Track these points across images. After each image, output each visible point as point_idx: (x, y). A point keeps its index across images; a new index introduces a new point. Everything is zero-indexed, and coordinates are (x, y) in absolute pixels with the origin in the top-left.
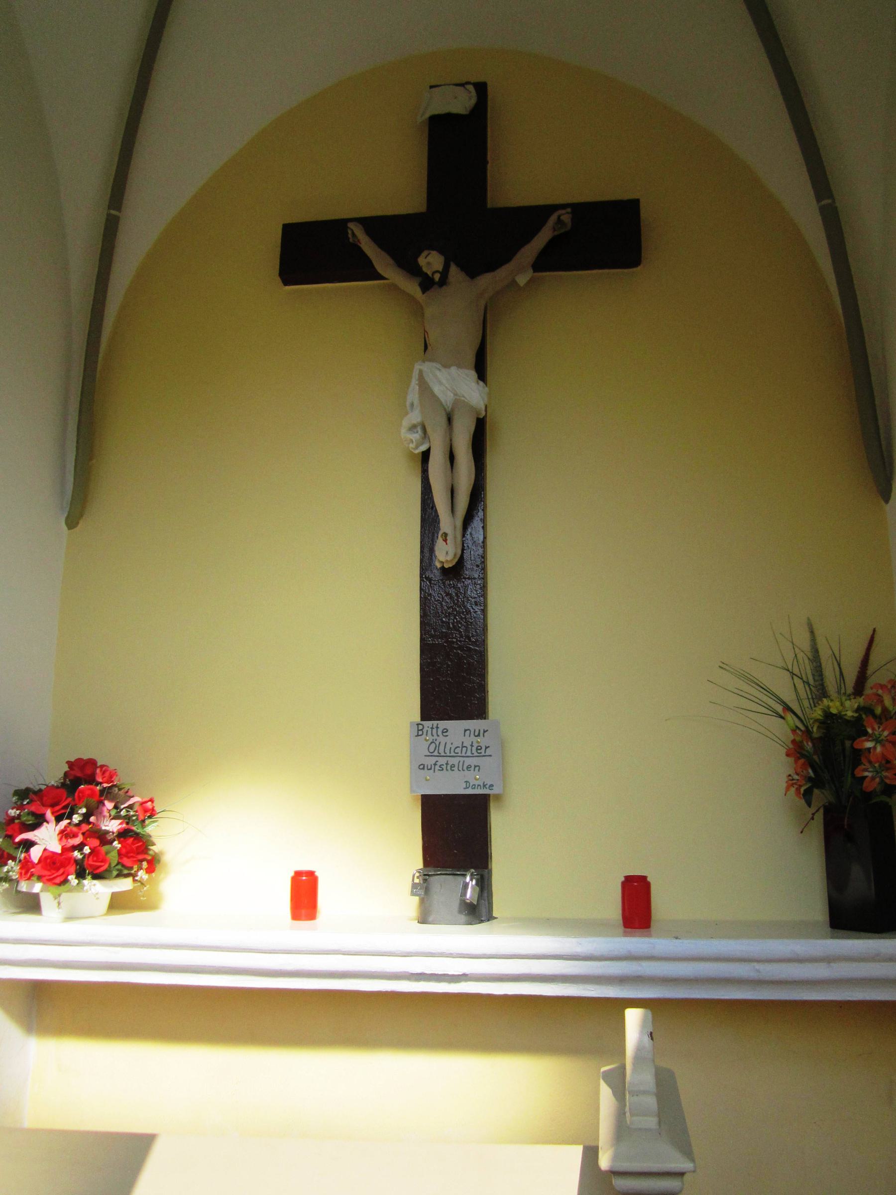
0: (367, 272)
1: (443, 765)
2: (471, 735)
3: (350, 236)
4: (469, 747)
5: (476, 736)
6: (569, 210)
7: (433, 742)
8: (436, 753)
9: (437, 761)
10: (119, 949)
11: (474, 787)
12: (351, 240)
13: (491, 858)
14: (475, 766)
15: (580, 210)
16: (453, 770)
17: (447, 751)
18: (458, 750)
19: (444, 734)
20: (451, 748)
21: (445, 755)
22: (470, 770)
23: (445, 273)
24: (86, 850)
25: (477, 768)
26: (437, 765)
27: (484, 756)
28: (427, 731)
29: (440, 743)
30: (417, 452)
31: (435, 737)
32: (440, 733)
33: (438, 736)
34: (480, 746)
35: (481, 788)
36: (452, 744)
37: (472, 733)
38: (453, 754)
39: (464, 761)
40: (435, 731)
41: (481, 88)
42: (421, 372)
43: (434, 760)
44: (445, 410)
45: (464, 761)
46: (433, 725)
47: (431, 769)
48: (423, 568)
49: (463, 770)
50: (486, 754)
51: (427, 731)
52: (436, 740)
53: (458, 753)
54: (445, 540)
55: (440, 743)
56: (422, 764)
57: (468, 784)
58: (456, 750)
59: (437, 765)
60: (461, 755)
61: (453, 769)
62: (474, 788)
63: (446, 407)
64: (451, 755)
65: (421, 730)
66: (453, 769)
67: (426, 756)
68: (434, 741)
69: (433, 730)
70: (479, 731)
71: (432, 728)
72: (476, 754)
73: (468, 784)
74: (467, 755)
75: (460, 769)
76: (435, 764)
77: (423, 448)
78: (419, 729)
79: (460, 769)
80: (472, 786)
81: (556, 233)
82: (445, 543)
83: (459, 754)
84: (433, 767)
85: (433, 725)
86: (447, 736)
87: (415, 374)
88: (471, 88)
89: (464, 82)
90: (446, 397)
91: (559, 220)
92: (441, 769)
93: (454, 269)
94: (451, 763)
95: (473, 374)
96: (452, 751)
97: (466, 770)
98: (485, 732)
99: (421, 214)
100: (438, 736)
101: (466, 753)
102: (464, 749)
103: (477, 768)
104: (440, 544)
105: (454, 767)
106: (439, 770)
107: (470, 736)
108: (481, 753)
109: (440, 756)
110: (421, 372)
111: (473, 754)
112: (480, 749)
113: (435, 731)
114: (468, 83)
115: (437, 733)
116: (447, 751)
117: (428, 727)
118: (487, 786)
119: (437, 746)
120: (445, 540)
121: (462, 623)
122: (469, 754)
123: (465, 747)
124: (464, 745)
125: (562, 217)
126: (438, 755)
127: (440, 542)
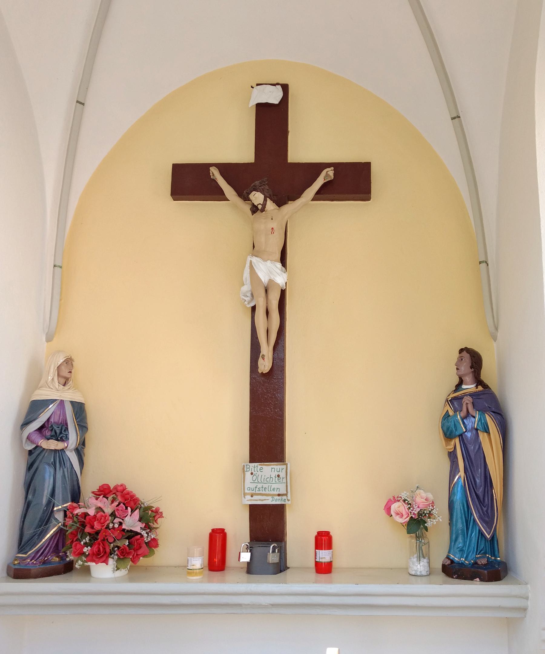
0: (219, 195)
1: (260, 488)
2: (275, 471)
3: (211, 174)
4: (274, 478)
5: (278, 472)
6: (332, 168)
7: (255, 475)
8: (256, 481)
9: (257, 486)
10: (79, 596)
11: (276, 500)
12: (212, 177)
13: (286, 535)
14: (277, 489)
15: (338, 167)
16: (266, 491)
17: (262, 480)
18: (268, 480)
19: (261, 470)
20: (264, 478)
21: (261, 482)
22: (275, 491)
23: (264, 205)
24: (116, 526)
25: (278, 490)
26: (257, 488)
27: (269, 483)
28: (252, 468)
29: (258, 475)
30: (249, 306)
31: (256, 472)
32: (258, 470)
33: (258, 472)
34: (262, 468)
35: (280, 501)
36: (265, 476)
37: (276, 469)
38: (265, 482)
39: (271, 486)
40: (256, 468)
41: (285, 88)
42: (251, 262)
43: (255, 485)
44: (264, 285)
45: (271, 486)
46: (255, 465)
47: (253, 490)
48: (252, 379)
49: (271, 491)
50: (283, 482)
51: (252, 468)
52: (256, 474)
53: (268, 481)
54: (264, 359)
55: (258, 475)
56: (249, 488)
57: (273, 498)
58: (267, 479)
59: (257, 488)
60: (270, 482)
61: (265, 490)
62: (277, 501)
63: (265, 284)
64: (264, 482)
65: (249, 468)
66: (265, 490)
67: (251, 483)
68: (256, 474)
69: (255, 468)
70: (280, 468)
71: (254, 467)
72: (278, 482)
73: (273, 498)
74: (273, 482)
75: (269, 490)
76: (256, 488)
77: (252, 304)
78: (248, 467)
79: (269, 490)
80: (276, 500)
81: (325, 181)
82: (263, 361)
83: (269, 482)
84: (255, 490)
85: (255, 465)
86: (262, 471)
87: (248, 265)
88: (279, 87)
89: (275, 83)
90: (264, 278)
91: (327, 175)
92: (259, 490)
93: (269, 202)
94: (258, 487)
95: (279, 265)
96: (265, 479)
97: (272, 491)
98: (282, 469)
99: (251, 163)
100: (258, 472)
101: (272, 482)
102: (271, 479)
103: (278, 490)
104: (260, 361)
105: (266, 489)
106: (258, 491)
107: (274, 472)
108: (280, 481)
109: (262, 483)
110: (251, 262)
111: (276, 482)
112: (280, 479)
113: (256, 468)
114: (278, 84)
115: (257, 470)
116: (262, 480)
117: (252, 466)
118: (283, 500)
119: (257, 477)
120: (264, 359)
121: (272, 404)
122: (274, 482)
123: (272, 478)
124: (271, 477)
125: (328, 173)
126: (275, 482)
127: (260, 360)
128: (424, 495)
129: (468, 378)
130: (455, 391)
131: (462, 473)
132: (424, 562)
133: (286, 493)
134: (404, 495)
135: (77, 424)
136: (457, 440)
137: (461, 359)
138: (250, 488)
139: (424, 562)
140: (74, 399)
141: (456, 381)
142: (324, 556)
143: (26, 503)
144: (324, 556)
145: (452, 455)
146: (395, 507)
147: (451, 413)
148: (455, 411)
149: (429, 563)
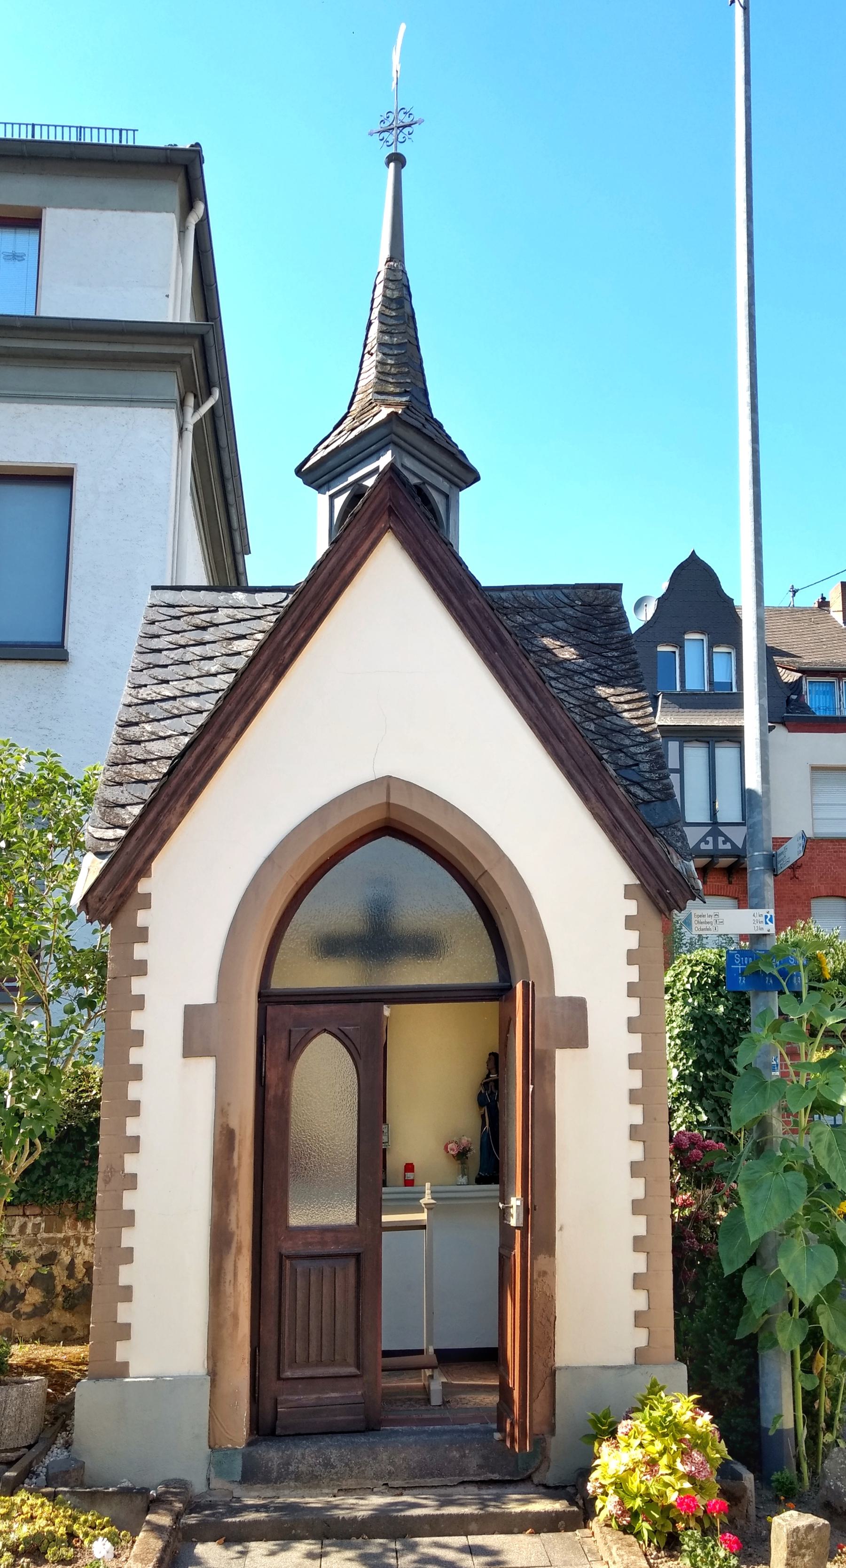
128: (466, 1139)
129: (493, 1071)
130: (486, 1079)
131: (487, 1126)
132: (465, 1177)
133: (277, 1433)
134: (455, 1139)
135: (212, 408)
136: (486, 1108)
137: (489, 1059)
138: (279, 1378)
139: (465, 1177)
140: (179, 503)
141: (487, 1072)
142: (410, 1176)
143: (189, 437)
144: (410, 1176)
145: (483, 1116)
146: (450, 1146)
147: (483, 1092)
148: (485, 1090)
149: (468, 1178)
